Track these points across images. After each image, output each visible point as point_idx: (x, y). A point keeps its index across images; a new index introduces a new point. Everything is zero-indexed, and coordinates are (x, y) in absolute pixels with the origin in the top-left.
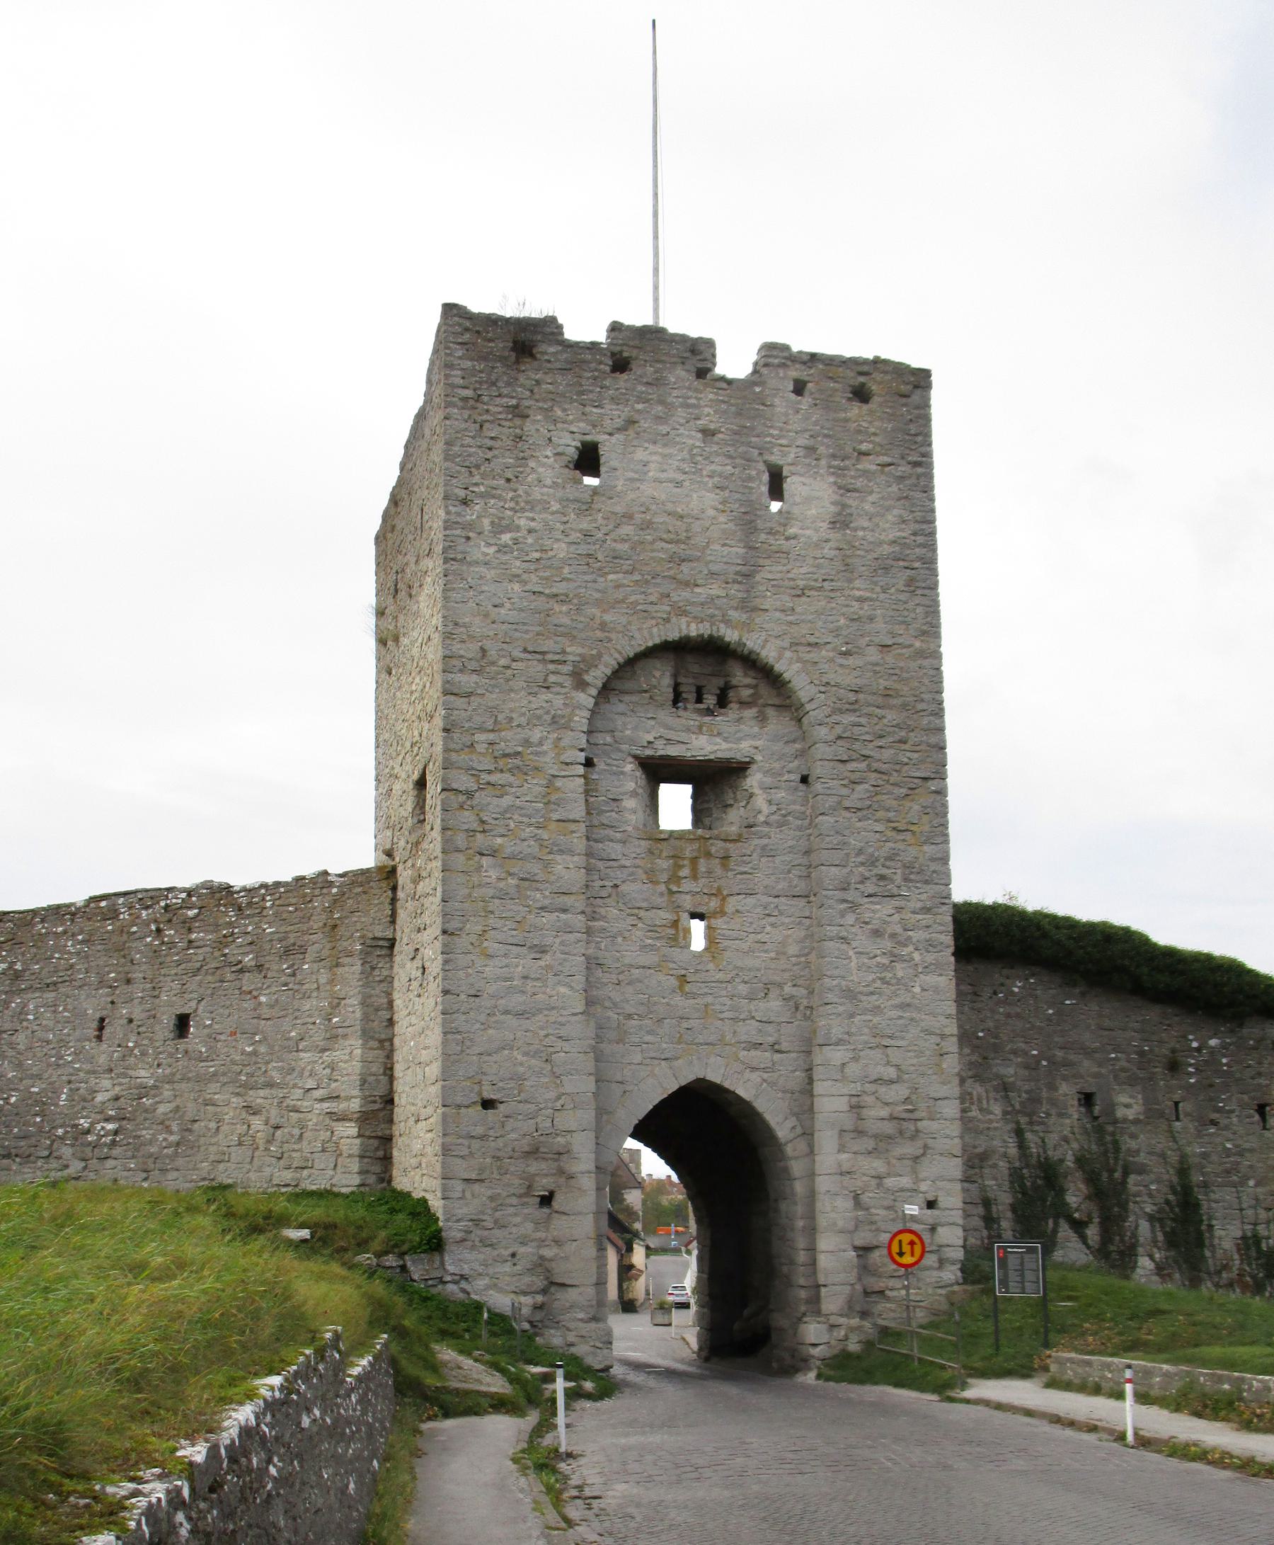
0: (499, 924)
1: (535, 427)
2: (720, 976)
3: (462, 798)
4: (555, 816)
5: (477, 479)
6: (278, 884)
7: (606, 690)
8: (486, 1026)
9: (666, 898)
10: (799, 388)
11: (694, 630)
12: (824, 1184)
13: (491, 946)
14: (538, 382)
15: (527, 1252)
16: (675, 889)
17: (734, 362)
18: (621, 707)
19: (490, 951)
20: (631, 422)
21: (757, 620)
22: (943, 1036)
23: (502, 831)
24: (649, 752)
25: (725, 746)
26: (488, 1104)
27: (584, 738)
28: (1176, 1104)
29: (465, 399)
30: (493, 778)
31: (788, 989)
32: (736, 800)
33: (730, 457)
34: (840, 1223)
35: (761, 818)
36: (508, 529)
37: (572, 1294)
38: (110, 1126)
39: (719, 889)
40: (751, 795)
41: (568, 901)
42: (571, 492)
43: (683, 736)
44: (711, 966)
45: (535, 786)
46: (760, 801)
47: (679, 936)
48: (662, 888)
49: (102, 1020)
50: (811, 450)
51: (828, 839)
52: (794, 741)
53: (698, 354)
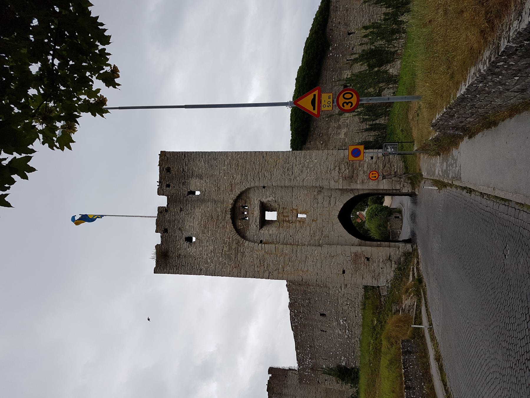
0: (300, 267)
1: (182, 252)
3: (270, 274)
5: (195, 267)
6: (289, 294)
7: (244, 237)
10: (168, 186)
11: (229, 216)
12: (365, 187)
13: (305, 269)
15: (381, 265)
17: (163, 201)
18: (248, 233)
20: (180, 229)
22: (328, 154)
26: (344, 272)
27: (256, 244)
28: (347, 60)
29: (177, 269)
30: (266, 267)
31: (315, 193)
34: (376, 183)
37: (392, 254)
41: (294, 250)
42: (197, 244)
43: (254, 218)
46: (270, 199)
47: (302, 220)
50: (183, 184)
53: (161, 210)
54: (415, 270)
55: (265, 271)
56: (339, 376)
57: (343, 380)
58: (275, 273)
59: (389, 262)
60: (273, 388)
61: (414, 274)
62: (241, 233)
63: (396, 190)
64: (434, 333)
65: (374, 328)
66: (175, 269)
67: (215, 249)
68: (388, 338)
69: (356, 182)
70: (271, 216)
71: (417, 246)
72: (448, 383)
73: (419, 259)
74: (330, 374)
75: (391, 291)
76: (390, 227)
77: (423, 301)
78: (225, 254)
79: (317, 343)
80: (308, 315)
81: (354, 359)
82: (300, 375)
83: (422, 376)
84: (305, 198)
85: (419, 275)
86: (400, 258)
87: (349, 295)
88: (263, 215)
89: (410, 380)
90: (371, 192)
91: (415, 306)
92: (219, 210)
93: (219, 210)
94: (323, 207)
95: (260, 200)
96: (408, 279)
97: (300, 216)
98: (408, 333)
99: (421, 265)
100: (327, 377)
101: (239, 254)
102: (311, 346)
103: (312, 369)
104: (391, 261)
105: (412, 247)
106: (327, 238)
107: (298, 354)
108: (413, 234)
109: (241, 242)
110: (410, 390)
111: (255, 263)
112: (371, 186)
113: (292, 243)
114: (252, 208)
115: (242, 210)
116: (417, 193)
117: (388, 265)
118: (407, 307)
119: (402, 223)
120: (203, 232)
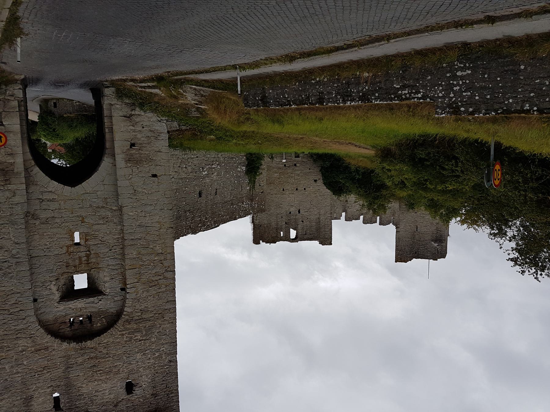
2: (67, 224)
4: (137, 269)
7: (119, 315)
8: (158, 200)
9: (91, 249)
11: (89, 343)
12: (19, 150)
14: (149, 407)
16: (88, 252)
18: (112, 310)
19: (158, 223)
20: (116, 406)
21: (63, 353)
23: (155, 262)
24: (101, 297)
25: (70, 306)
26: (154, 176)
30: (159, 277)
31: (37, 222)
32: (62, 287)
33: (77, 407)
34: (11, 135)
35: (54, 283)
36: (157, 357)
37: (121, 114)
38: (214, 166)
39: (70, 255)
40: (58, 290)
41: (131, 243)
44: (71, 227)
45: (144, 278)
46: (54, 289)
48: (92, 252)
49: (200, 196)
51: (27, 280)
52: (41, 313)
54: (143, 84)
55: (165, 278)
56: (256, 173)
57: (258, 168)
58: (166, 264)
59: (134, 117)
60: (272, 237)
61: (149, 87)
62: (113, 320)
63: (19, 106)
64: (248, 64)
65: (219, 138)
66: (173, 395)
67: (140, 351)
68: (240, 123)
69: (12, 164)
70: (81, 282)
71: (107, 81)
72: (337, 45)
73: (127, 79)
74: (255, 181)
75: (172, 117)
76: (71, 114)
77: (192, 76)
78: (146, 335)
79: (228, 198)
80: (202, 211)
81: (238, 157)
82: (258, 212)
83: (300, 82)
84: (47, 237)
85: (151, 79)
86: (126, 104)
87: (175, 166)
88: (82, 293)
89: (308, 98)
90: (26, 141)
91: (197, 87)
92: (80, 360)
93: (80, 360)
94: (60, 209)
95: (58, 302)
96: (156, 95)
97: (77, 239)
98: (234, 98)
99: (136, 77)
100: (257, 184)
101: (144, 316)
102: (232, 204)
103: (252, 200)
104: (131, 115)
105: (108, 87)
106: (108, 200)
107: (241, 217)
108: (83, 86)
109: (127, 317)
110: (324, 98)
111: (154, 292)
112: (16, 140)
113: (121, 246)
114: (72, 312)
115: (76, 326)
116: (23, 77)
117: (137, 120)
118: (196, 98)
119: (63, 99)
120: (118, 373)
